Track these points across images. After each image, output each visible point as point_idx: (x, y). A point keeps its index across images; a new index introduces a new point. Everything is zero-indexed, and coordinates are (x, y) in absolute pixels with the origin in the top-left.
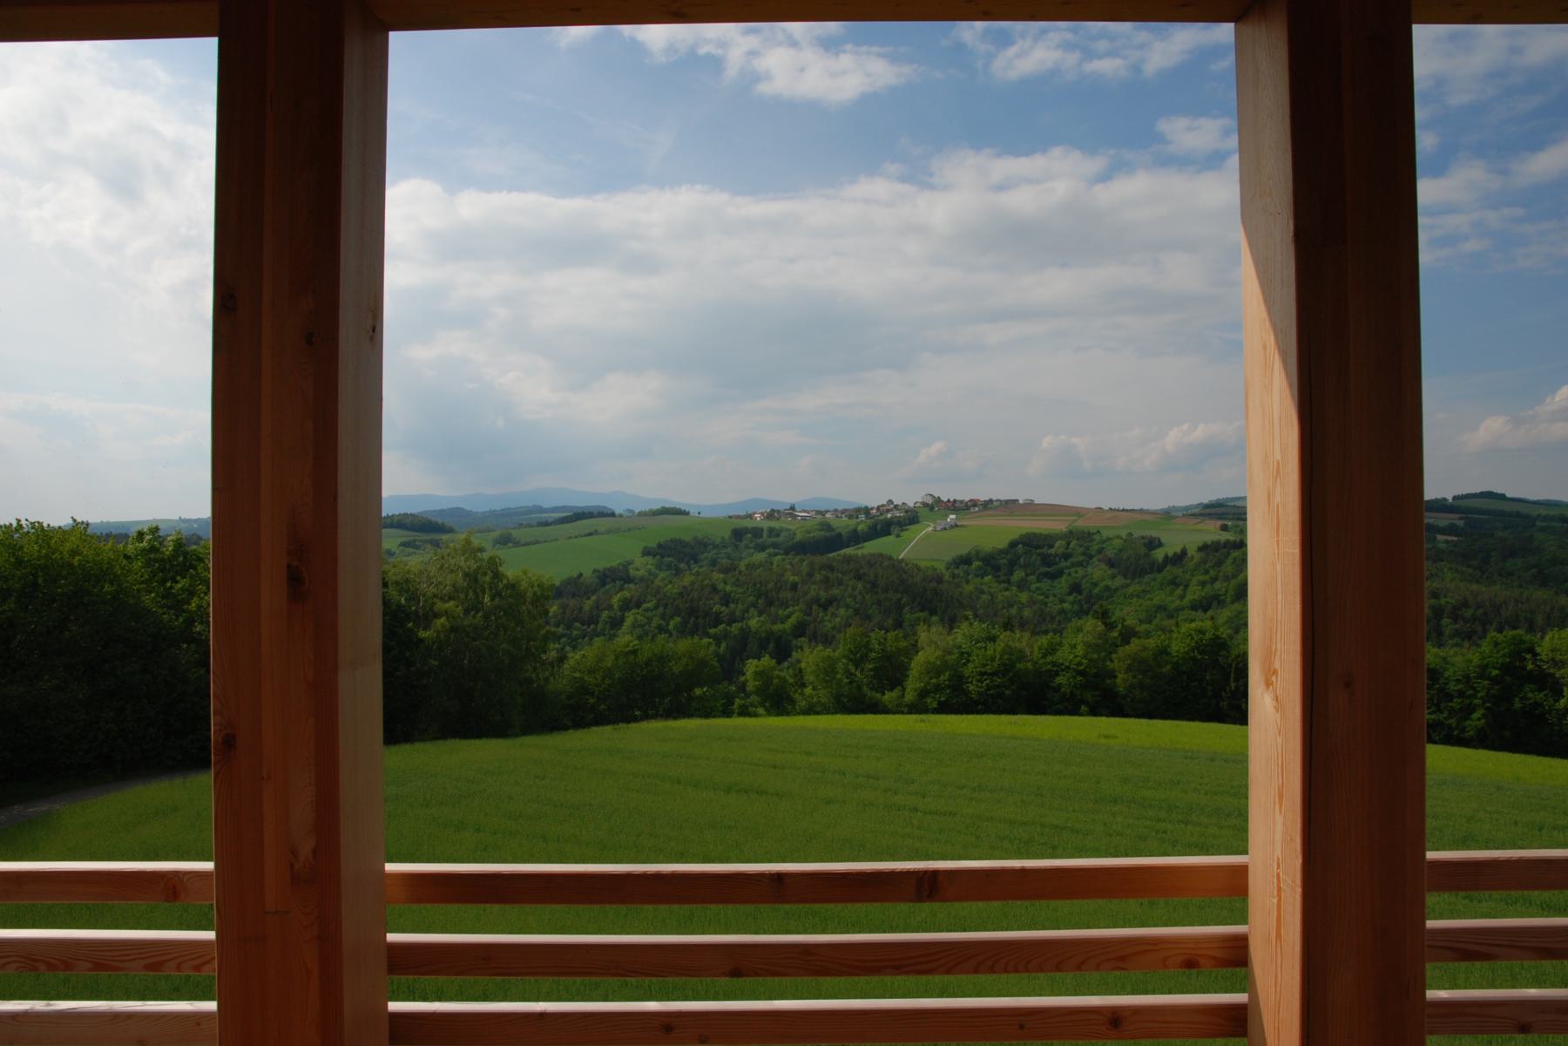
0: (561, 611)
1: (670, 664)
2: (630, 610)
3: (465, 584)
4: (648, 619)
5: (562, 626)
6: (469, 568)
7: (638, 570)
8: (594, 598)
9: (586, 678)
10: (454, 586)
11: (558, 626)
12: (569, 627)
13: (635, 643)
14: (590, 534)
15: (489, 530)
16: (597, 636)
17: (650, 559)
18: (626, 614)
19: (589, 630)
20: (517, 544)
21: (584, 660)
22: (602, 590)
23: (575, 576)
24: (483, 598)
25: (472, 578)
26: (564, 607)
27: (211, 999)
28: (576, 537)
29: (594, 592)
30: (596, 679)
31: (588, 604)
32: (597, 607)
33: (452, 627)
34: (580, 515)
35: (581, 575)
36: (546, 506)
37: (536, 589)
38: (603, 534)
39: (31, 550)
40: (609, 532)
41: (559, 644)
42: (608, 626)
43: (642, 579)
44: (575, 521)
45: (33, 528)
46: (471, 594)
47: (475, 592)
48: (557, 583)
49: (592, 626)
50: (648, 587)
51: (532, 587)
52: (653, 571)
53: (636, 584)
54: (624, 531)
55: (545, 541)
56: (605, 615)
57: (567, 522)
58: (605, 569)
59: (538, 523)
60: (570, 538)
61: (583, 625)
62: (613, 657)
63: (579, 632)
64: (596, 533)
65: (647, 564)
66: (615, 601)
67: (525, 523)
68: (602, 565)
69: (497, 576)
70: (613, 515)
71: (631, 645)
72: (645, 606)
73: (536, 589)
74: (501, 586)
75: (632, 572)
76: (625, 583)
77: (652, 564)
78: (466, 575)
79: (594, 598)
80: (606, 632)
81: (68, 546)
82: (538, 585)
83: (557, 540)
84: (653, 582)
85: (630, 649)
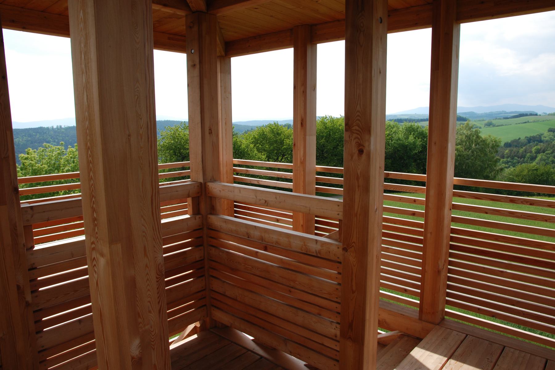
0: (510, 152)
1: (552, 176)
2: (540, 153)
3: (465, 140)
4: (547, 157)
5: (509, 158)
6: (467, 134)
7: (545, 137)
8: (524, 148)
9: (515, 178)
10: (461, 140)
11: (508, 158)
12: (513, 159)
13: (537, 166)
14: (525, 123)
15: (483, 120)
16: (524, 163)
17: (552, 133)
18: (538, 155)
19: (521, 160)
20: (494, 126)
21: (515, 171)
22: (528, 145)
23: (517, 139)
24: (472, 145)
25: (468, 137)
26: (511, 151)
27: (18, 179)
28: (519, 123)
29: (524, 146)
30: (519, 179)
31: (521, 150)
32: (525, 152)
33: (459, 155)
34: (522, 115)
35: (520, 139)
36: (507, 111)
37: (493, 143)
38: (531, 122)
39: (329, 125)
40: (534, 122)
41: (508, 165)
42: (529, 159)
43: (547, 141)
44: (520, 117)
45: (330, 118)
46: (468, 143)
47: (469, 143)
48: (509, 141)
49: (522, 159)
50: (549, 144)
51: (492, 142)
52: (552, 138)
53: (544, 143)
54: (540, 122)
55: (506, 125)
56: (528, 155)
57: (516, 118)
58: (530, 137)
59: (503, 118)
60: (517, 124)
61: (519, 158)
62: (527, 171)
63: (517, 161)
64: (528, 122)
65: (550, 135)
66: (533, 150)
67: (498, 118)
68: (529, 135)
69: (478, 137)
70: (536, 115)
71: (535, 167)
72: (547, 152)
73: (493, 143)
74: (479, 141)
75: (543, 138)
76: (539, 143)
77: (552, 135)
78: (466, 136)
79: (524, 148)
80: (529, 161)
81: (339, 123)
82: (494, 141)
83: (511, 124)
84: (551, 143)
85: (535, 168)
